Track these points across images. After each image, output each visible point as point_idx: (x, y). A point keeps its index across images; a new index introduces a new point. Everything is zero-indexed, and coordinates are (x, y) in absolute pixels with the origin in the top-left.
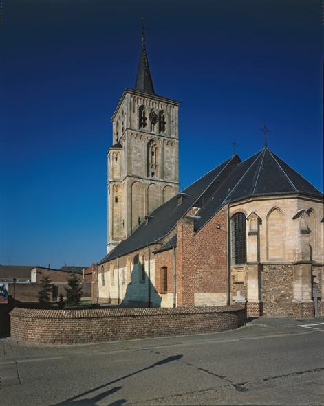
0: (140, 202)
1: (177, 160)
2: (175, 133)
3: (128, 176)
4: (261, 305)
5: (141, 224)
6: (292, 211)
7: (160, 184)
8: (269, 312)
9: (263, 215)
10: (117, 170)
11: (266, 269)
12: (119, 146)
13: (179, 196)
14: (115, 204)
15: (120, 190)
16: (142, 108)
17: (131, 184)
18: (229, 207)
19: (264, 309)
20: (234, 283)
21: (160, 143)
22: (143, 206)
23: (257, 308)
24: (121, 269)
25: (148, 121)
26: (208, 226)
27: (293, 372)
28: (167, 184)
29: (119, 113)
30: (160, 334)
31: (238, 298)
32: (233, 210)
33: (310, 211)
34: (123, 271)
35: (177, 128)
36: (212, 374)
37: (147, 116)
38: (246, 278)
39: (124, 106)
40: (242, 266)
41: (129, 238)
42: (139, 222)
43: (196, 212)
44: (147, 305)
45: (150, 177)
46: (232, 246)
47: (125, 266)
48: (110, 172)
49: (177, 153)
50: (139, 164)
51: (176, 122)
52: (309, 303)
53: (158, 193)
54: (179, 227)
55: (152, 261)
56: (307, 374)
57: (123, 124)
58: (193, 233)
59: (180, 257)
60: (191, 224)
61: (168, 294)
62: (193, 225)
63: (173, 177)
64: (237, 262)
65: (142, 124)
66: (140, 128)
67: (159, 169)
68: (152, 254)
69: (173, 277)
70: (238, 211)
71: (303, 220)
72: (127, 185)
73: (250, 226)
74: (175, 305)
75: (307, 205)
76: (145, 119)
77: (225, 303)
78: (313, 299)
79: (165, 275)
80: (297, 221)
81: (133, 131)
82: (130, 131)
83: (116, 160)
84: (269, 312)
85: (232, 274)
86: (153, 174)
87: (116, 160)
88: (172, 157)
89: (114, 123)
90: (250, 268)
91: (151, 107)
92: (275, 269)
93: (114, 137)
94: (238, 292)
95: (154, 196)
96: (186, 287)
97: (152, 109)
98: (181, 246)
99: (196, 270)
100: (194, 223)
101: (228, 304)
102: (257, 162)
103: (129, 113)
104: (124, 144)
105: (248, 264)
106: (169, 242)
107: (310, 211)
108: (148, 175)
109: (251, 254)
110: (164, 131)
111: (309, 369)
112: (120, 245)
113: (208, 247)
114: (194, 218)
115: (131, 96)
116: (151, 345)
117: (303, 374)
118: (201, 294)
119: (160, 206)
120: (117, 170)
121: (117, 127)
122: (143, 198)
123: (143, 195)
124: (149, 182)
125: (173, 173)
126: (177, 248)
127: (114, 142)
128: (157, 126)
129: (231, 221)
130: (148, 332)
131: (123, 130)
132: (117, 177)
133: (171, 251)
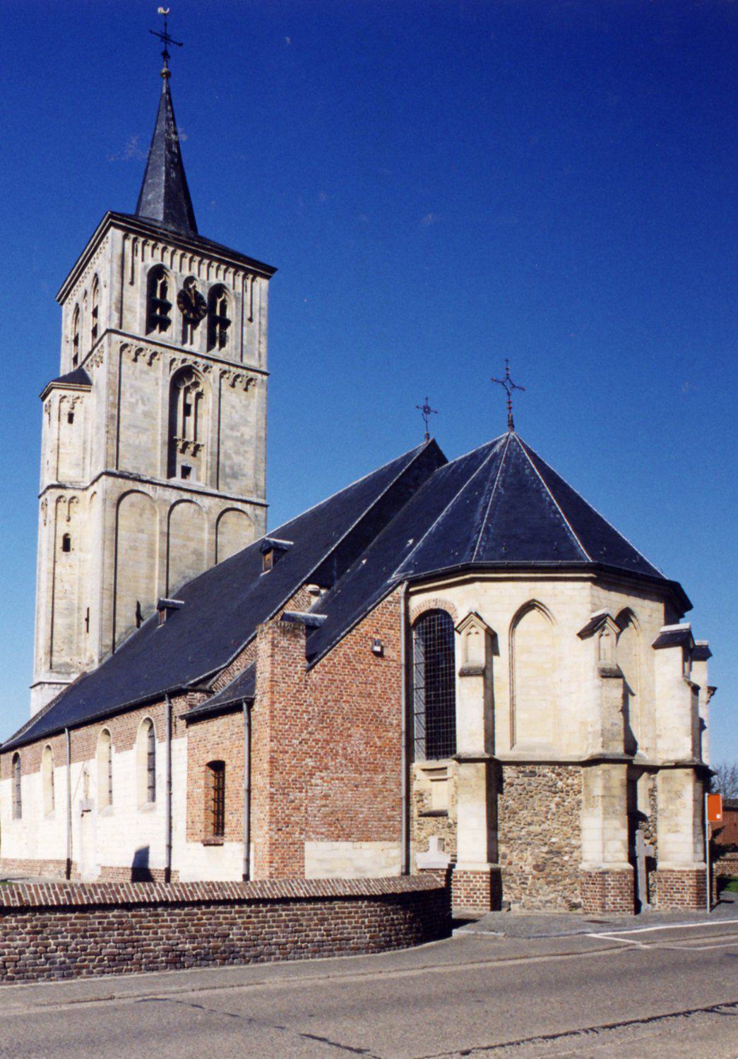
0: (143, 553)
1: (263, 434)
2: (257, 357)
3: (108, 474)
4: (496, 879)
5: (142, 624)
7: (206, 502)
8: (518, 899)
9: (501, 625)
10: (71, 452)
11: (508, 772)
12: (80, 379)
13: (264, 547)
15: (79, 513)
17: (116, 496)
18: (408, 595)
19: (505, 889)
20: (422, 815)
21: (209, 382)
22: (152, 567)
23: (483, 885)
24: (77, 767)
25: (175, 314)
26: (349, 646)
27: (536, 1034)
28: (229, 504)
29: (86, 282)
30: (204, 958)
31: (430, 858)
32: (421, 602)
33: (625, 618)
35: (263, 340)
36: (338, 1045)
37: (172, 297)
38: (454, 800)
39: (104, 263)
40: (442, 763)
41: (104, 668)
42: (139, 617)
43: (315, 600)
45: (177, 480)
46: (419, 706)
47: (92, 756)
48: (47, 456)
49: (262, 414)
50: (144, 438)
51: (261, 321)
52: (621, 873)
53: (201, 529)
54: (263, 645)
55: (180, 744)
56: (567, 1039)
57: (95, 313)
58: (303, 663)
59: (263, 733)
60: (296, 636)
62: (303, 642)
63: (248, 482)
64: (432, 753)
65: (156, 318)
66: (148, 331)
67: (204, 455)
68: (181, 724)
69: (243, 795)
70: (433, 606)
71: (605, 640)
72: (104, 500)
73: (468, 649)
74: (246, 877)
75: (615, 601)
76: (167, 307)
77: (396, 871)
78: (632, 859)
79: (220, 789)
80: (592, 641)
81: (126, 340)
82: (115, 337)
84: (518, 899)
85: (415, 787)
86: (186, 471)
88: (246, 422)
89: (68, 309)
90: (466, 770)
91: (186, 273)
92: (533, 774)
93: (67, 352)
94: (433, 841)
96: (280, 824)
97: (190, 280)
98: (266, 701)
99: (311, 775)
100: (307, 635)
101: (407, 873)
102: (487, 470)
103: (118, 286)
104: (98, 374)
105: (461, 760)
106: (234, 688)
107: (625, 618)
108: (171, 473)
109: (469, 737)
110: (223, 344)
111: (572, 1029)
112: (72, 688)
113: (346, 706)
114: (306, 619)
115: (125, 237)
116: (174, 988)
117: (558, 1040)
119: (205, 568)
120: (71, 452)
121: (76, 320)
122: (151, 545)
123: (153, 535)
124: (173, 496)
125: (249, 469)
126: (256, 707)
127: (66, 367)
128: (200, 332)
129: (414, 635)
130: (166, 951)
131: (94, 332)
133: (240, 718)
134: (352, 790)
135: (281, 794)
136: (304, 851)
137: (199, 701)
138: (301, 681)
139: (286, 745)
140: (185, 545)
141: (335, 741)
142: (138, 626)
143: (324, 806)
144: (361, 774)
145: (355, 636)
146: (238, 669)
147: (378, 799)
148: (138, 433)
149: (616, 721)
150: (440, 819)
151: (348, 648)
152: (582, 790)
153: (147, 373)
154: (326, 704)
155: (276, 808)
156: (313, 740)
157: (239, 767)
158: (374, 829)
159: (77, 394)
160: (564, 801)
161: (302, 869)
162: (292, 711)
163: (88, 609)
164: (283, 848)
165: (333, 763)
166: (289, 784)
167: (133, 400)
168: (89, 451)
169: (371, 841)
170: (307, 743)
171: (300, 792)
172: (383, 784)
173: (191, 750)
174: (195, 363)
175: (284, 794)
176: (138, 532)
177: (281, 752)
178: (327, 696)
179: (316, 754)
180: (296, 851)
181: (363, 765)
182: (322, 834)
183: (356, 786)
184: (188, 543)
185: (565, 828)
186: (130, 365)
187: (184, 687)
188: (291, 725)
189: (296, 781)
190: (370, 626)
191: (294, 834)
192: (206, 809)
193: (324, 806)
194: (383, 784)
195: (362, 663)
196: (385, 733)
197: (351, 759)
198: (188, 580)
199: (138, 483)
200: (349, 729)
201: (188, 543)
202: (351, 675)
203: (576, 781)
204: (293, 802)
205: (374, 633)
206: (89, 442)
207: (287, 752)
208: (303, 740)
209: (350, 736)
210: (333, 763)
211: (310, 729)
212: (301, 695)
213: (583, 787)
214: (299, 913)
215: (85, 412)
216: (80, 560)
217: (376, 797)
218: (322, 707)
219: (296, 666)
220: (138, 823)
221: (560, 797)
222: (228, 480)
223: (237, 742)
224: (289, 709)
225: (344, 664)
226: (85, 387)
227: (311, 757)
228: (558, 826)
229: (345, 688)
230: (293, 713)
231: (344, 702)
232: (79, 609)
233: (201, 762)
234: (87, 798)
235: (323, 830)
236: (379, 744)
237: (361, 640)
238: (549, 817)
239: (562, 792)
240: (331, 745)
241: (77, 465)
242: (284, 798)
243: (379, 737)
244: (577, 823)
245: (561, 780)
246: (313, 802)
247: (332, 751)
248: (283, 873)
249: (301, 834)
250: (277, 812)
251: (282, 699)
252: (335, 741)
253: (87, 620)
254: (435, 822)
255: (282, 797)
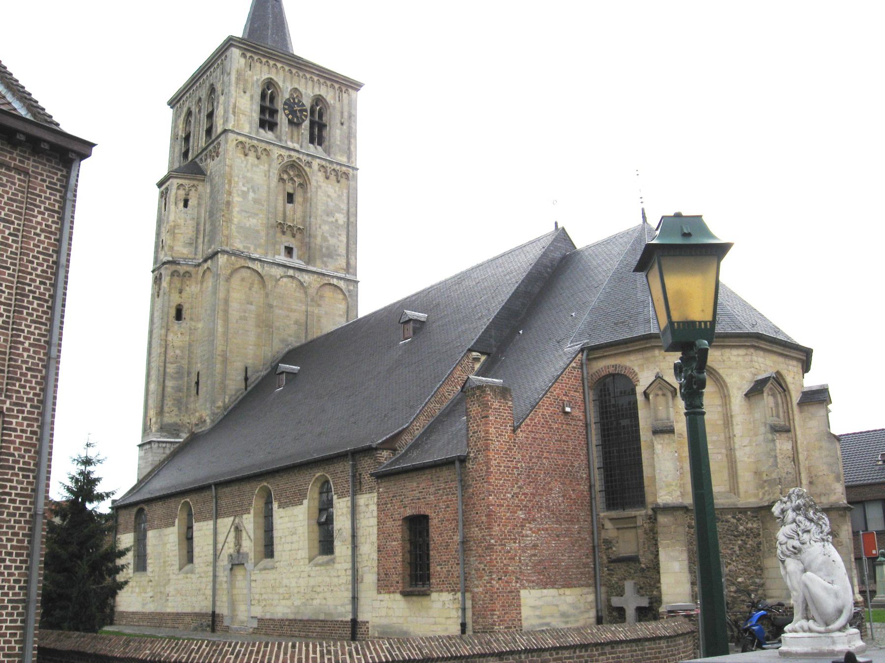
5: (249, 389)
6: (743, 378)
14: (176, 326)
16: (270, 84)
24: (225, 523)
28: (326, 280)
34: (238, 530)
42: (246, 379)
43: (477, 366)
44: (348, 632)
61: (434, 596)
65: (267, 121)
70: (611, 370)
74: (463, 626)
83: (186, 205)
87: (186, 205)
94: (629, 585)
95: (291, 310)
99: (523, 526)
118: (536, 593)
131: (209, 132)
132: (185, 251)
134: (555, 540)
135: (499, 545)
136: (519, 599)
137: (386, 460)
138: (510, 439)
139: (502, 499)
140: (288, 316)
141: (540, 495)
142: (246, 389)
143: (535, 555)
144: (561, 525)
145: (549, 398)
146: (418, 429)
147: (576, 548)
148: (248, 217)
149: (790, 471)
150: (632, 565)
151: (546, 409)
152: (761, 533)
153: (257, 166)
154: (531, 460)
155: (496, 559)
156: (523, 494)
157: (448, 520)
158: (574, 576)
159: (192, 183)
160: (746, 544)
161: (519, 616)
162: (505, 467)
163: (198, 373)
164: (503, 596)
165: (539, 515)
166: (505, 535)
167: (245, 189)
168: (202, 232)
169: (572, 587)
170: (517, 497)
171: (515, 542)
172: (579, 533)
173: (382, 507)
174: (298, 158)
175: (502, 545)
176: (248, 303)
177: (498, 506)
178: (531, 453)
179: (525, 506)
180: (513, 599)
181: (562, 516)
182: (533, 582)
183: (558, 536)
184: (290, 314)
185: (749, 568)
186: (243, 159)
187: (374, 446)
188: (505, 480)
189: (511, 532)
190: (560, 389)
191: (511, 582)
192: (403, 561)
193: (535, 555)
194: (579, 533)
195: (556, 423)
196: (578, 486)
197: (553, 511)
198: (290, 347)
199: (248, 261)
200: (549, 483)
201: (290, 314)
202: (548, 434)
203: (755, 525)
204: (509, 552)
205: (564, 395)
206: (202, 224)
207: (503, 506)
208: (514, 493)
209: (551, 489)
210: (539, 515)
211: (519, 484)
212: (511, 452)
213: (761, 530)
214: (621, 655)
215: (199, 198)
216: (190, 329)
217: (574, 546)
218: (528, 463)
219: (506, 426)
220: (309, 576)
221: (742, 540)
222: (325, 259)
223: (444, 497)
224: (503, 465)
225: (543, 424)
226: (199, 177)
227: (521, 510)
228: (742, 567)
229: (545, 446)
230: (506, 469)
231: (545, 458)
232: (189, 373)
233: (396, 516)
234: (238, 552)
235: (535, 578)
236: (573, 496)
237: (555, 402)
238: (734, 559)
239: (743, 535)
240: (537, 499)
241: (191, 244)
242: (503, 549)
243: (573, 490)
244: (759, 563)
245: (741, 524)
246: (525, 552)
247: (537, 504)
248: (505, 621)
249: (517, 582)
250: (497, 562)
251: (496, 456)
252: (540, 495)
253: (197, 383)
254: (626, 568)
255: (500, 548)
